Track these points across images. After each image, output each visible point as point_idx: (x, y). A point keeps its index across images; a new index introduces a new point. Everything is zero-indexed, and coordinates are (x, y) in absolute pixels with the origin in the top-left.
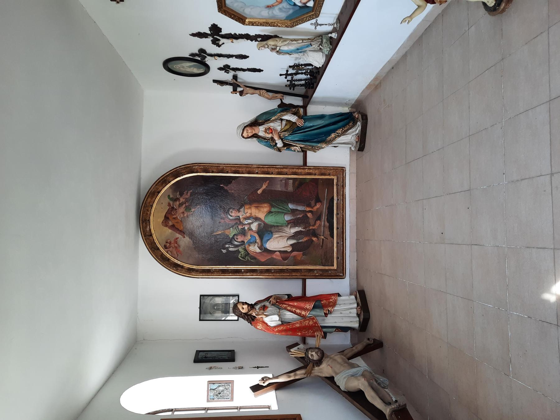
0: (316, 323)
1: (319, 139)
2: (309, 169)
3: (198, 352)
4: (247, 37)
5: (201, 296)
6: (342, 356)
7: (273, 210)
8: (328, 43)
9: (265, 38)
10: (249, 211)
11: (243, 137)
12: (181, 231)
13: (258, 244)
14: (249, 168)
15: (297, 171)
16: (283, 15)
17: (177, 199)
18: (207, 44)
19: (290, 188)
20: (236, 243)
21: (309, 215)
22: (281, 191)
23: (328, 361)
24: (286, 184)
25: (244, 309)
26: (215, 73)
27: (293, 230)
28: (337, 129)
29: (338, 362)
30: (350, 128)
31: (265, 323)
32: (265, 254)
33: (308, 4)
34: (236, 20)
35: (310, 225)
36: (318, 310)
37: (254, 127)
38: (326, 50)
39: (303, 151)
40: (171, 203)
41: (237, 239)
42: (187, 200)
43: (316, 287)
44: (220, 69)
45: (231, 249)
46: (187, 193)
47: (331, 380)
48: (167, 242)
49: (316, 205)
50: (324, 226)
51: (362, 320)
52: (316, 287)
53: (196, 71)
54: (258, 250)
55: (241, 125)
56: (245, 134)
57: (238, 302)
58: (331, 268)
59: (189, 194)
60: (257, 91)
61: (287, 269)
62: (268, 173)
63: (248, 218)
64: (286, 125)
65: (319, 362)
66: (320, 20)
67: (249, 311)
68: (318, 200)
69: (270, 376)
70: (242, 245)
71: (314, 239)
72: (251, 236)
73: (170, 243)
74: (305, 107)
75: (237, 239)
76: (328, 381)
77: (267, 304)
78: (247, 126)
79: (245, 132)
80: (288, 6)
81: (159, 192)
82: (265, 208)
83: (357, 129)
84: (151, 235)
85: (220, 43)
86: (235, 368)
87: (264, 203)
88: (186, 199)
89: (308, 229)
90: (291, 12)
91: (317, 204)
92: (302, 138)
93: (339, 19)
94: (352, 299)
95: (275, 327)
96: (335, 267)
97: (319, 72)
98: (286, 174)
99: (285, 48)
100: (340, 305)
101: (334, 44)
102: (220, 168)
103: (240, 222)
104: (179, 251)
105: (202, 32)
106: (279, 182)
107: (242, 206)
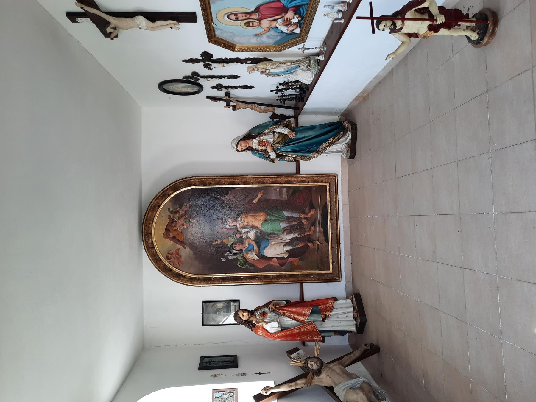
0: (314, 328)
1: (311, 149)
2: (302, 177)
3: (202, 358)
4: (238, 60)
5: (203, 302)
6: (341, 366)
7: (269, 218)
8: (316, 64)
9: (256, 61)
10: (246, 220)
11: (238, 151)
12: (181, 242)
13: (256, 251)
14: (244, 178)
15: (290, 179)
16: (271, 41)
17: (177, 212)
18: (199, 68)
19: (285, 197)
20: (235, 251)
21: (304, 221)
22: (276, 200)
23: (327, 372)
24: (281, 193)
25: (245, 316)
26: (208, 91)
27: (289, 237)
28: (327, 139)
29: (337, 373)
30: (341, 138)
31: (265, 329)
32: (263, 261)
33: (295, 31)
34: (226, 48)
35: (305, 232)
36: (316, 315)
37: (247, 141)
38: (315, 71)
39: (295, 161)
40: (171, 215)
41: (235, 247)
42: (186, 212)
43: (314, 291)
44: (213, 88)
45: (230, 258)
46: (186, 205)
47: (330, 389)
48: (168, 254)
49: (310, 212)
50: (319, 232)
51: (358, 324)
52: (314, 291)
53: (190, 90)
54: (256, 258)
55: (235, 139)
56: (239, 148)
57: (239, 309)
58: (327, 272)
59: (188, 207)
60: (250, 106)
61: (285, 275)
62: (263, 183)
63: (245, 227)
64: (278, 137)
65: (318, 372)
66: (307, 44)
67: (249, 318)
68: (312, 207)
69: (271, 384)
70: (240, 253)
71: (310, 244)
72: (249, 244)
73: (172, 254)
74: (296, 117)
75: (235, 247)
76: (328, 390)
77: (266, 310)
78: (241, 140)
79: (239, 146)
80: (276, 34)
81: (159, 206)
82: (261, 217)
83: (348, 138)
84: (154, 247)
85: (212, 68)
86: (238, 375)
87: (261, 211)
88: (186, 211)
89: (303, 235)
90: (279, 38)
91: (311, 210)
92: (294, 149)
93: (325, 42)
94: (348, 303)
95: (275, 333)
96: (331, 271)
97: (308, 88)
98: (280, 183)
99: (275, 71)
100: (337, 309)
101: (322, 66)
102: (216, 179)
103: (238, 231)
104: (181, 261)
105: (194, 58)
106: (274, 191)
107: (239, 215)
